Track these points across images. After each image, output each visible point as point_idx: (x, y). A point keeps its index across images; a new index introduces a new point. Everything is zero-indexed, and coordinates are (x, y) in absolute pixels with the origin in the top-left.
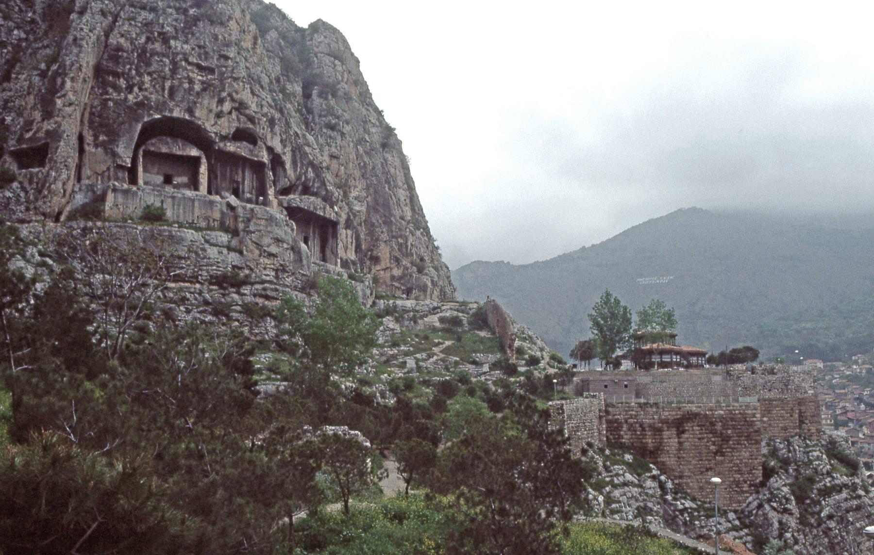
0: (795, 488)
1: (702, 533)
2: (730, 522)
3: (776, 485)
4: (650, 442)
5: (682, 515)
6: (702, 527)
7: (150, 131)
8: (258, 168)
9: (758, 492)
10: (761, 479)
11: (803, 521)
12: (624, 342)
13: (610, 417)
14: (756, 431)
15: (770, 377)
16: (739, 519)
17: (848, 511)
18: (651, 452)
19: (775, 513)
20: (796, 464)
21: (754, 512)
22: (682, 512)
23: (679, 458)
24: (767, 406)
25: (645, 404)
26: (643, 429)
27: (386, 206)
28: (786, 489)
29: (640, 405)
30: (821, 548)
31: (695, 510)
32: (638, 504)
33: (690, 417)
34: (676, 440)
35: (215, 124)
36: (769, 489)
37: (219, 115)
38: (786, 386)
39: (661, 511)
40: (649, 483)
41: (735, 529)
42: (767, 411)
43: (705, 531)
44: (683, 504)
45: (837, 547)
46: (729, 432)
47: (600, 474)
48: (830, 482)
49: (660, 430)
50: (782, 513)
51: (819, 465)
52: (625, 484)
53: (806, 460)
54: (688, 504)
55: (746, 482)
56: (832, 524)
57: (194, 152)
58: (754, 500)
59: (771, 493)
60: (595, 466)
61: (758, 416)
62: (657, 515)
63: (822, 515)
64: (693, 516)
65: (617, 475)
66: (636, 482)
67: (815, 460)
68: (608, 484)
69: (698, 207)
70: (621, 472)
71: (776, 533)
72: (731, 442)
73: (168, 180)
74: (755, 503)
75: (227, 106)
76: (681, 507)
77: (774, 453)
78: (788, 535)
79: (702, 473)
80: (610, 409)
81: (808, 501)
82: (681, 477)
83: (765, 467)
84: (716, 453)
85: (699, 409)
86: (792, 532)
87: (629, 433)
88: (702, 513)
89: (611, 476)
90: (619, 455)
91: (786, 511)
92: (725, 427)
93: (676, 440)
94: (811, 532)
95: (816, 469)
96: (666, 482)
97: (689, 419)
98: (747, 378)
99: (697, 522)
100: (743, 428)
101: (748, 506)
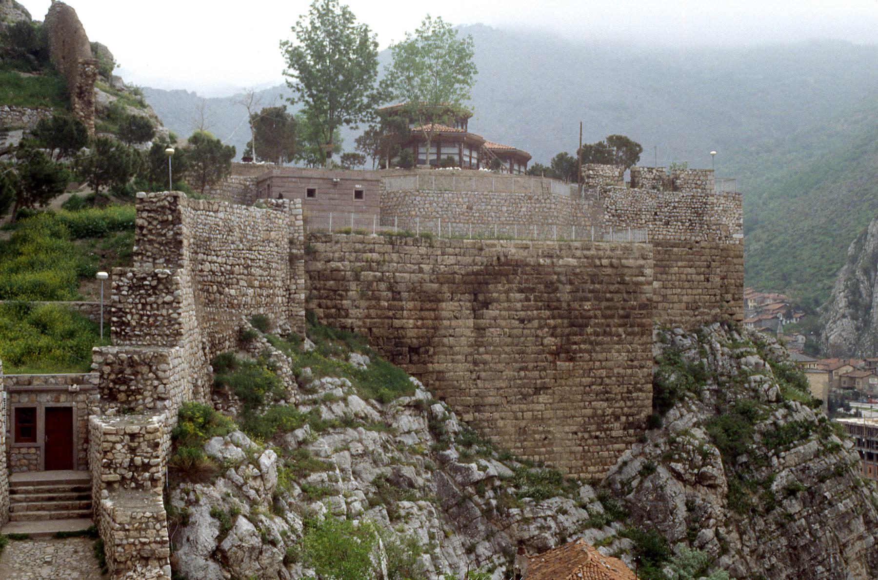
0: (718, 430)
1: (526, 536)
2: (584, 507)
3: (680, 425)
4: (410, 325)
5: (481, 494)
6: (526, 521)
9: (642, 441)
10: (649, 411)
11: (733, 500)
12: (360, 110)
13: (319, 265)
14: (643, 307)
15: (668, 196)
16: (602, 499)
17: (822, 480)
18: (414, 350)
19: (680, 485)
20: (715, 379)
21: (635, 483)
22: (480, 486)
23: (475, 363)
24: (664, 253)
25: (401, 236)
26: (396, 295)
28: (699, 433)
29: (391, 239)
30: (774, 560)
31: (509, 480)
32: (377, 471)
33: (502, 269)
34: (471, 322)
36: (666, 433)
38: (699, 215)
39: (434, 486)
40: (407, 421)
41: (594, 523)
42: (662, 267)
43: (532, 530)
44: (484, 469)
45: (805, 556)
46: (587, 305)
47: (283, 396)
48: (785, 417)
49: (435, 299)
50: (694, 485)
51: (761, 382)
52: (348, 422)
53: (735, 372)
54: (495, 468)
55: (617, 418)
56: (794, 506)
58: (635, 457)
59: (672, 442)
60: (270, 374)
61: (648, 271)
62: (425, 498)
63: (774, 487)
64: (506, 495)
65: (329, 400)
66: (376, 416)
67: (754, 373)
68: (302, 420)
69: (486, 24)
70: (339, 392)
71: (681, 530)
72: (589, 330)
74: (637, 465)
76: (478, 475)
77: (672, 358)
78: (709, 533)
79: (525, 397)
80: (320, 246)
81: (744, 459)
82: (478, 408)
83: (658, 389)
84: (556, 354)
85: (524, 253)
86: (716, 526)
87: (364, 304)
88: (525, 489)
89: (315, 402)
90: (336, 354)
91: (702, 479)
93: (471, 322)
94: (753, 525)
95: (755, 391)
96: (444, 419)
97: (500, 273)
98: (621, 196)
99: (514, 511)
100: (616, 297)
101: (620, 471)
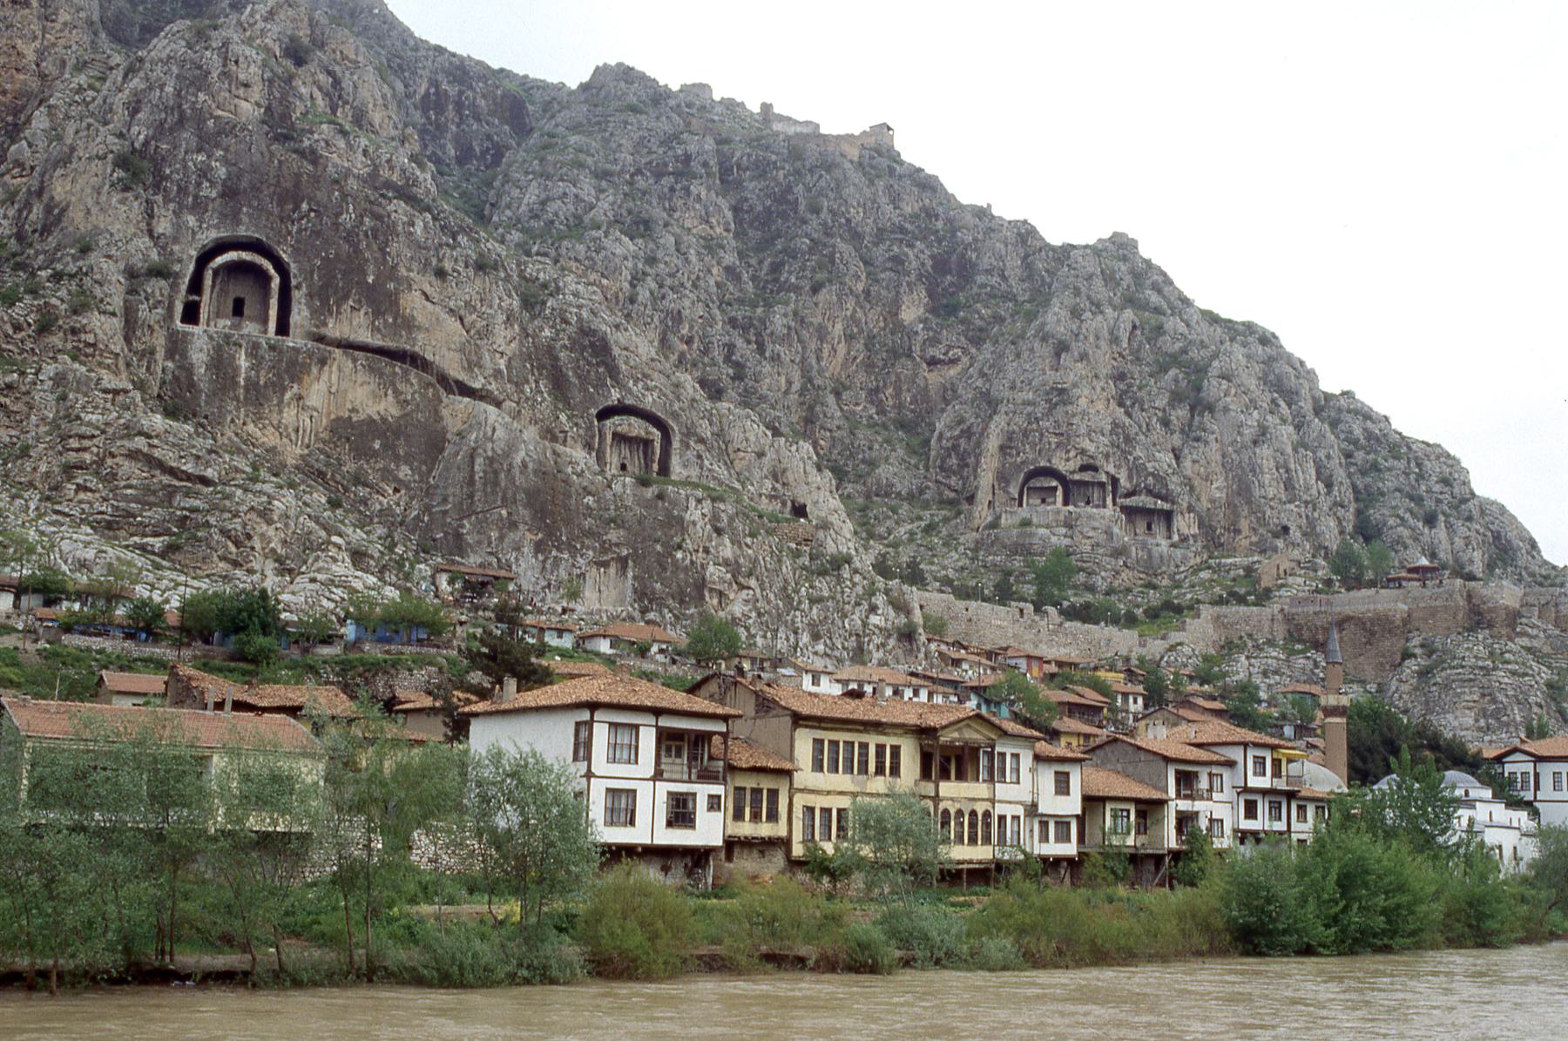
4: (1320, 637)
7: (1031, 475)
8: (1102, 485)
27: (1248, 490)
33: (1348, 619)
35: (1065, 464)
37: (1068, 460)
57: (1054, 484)
73: (1043, 501)
75: (1072, 454)
92: (1372, 625)
